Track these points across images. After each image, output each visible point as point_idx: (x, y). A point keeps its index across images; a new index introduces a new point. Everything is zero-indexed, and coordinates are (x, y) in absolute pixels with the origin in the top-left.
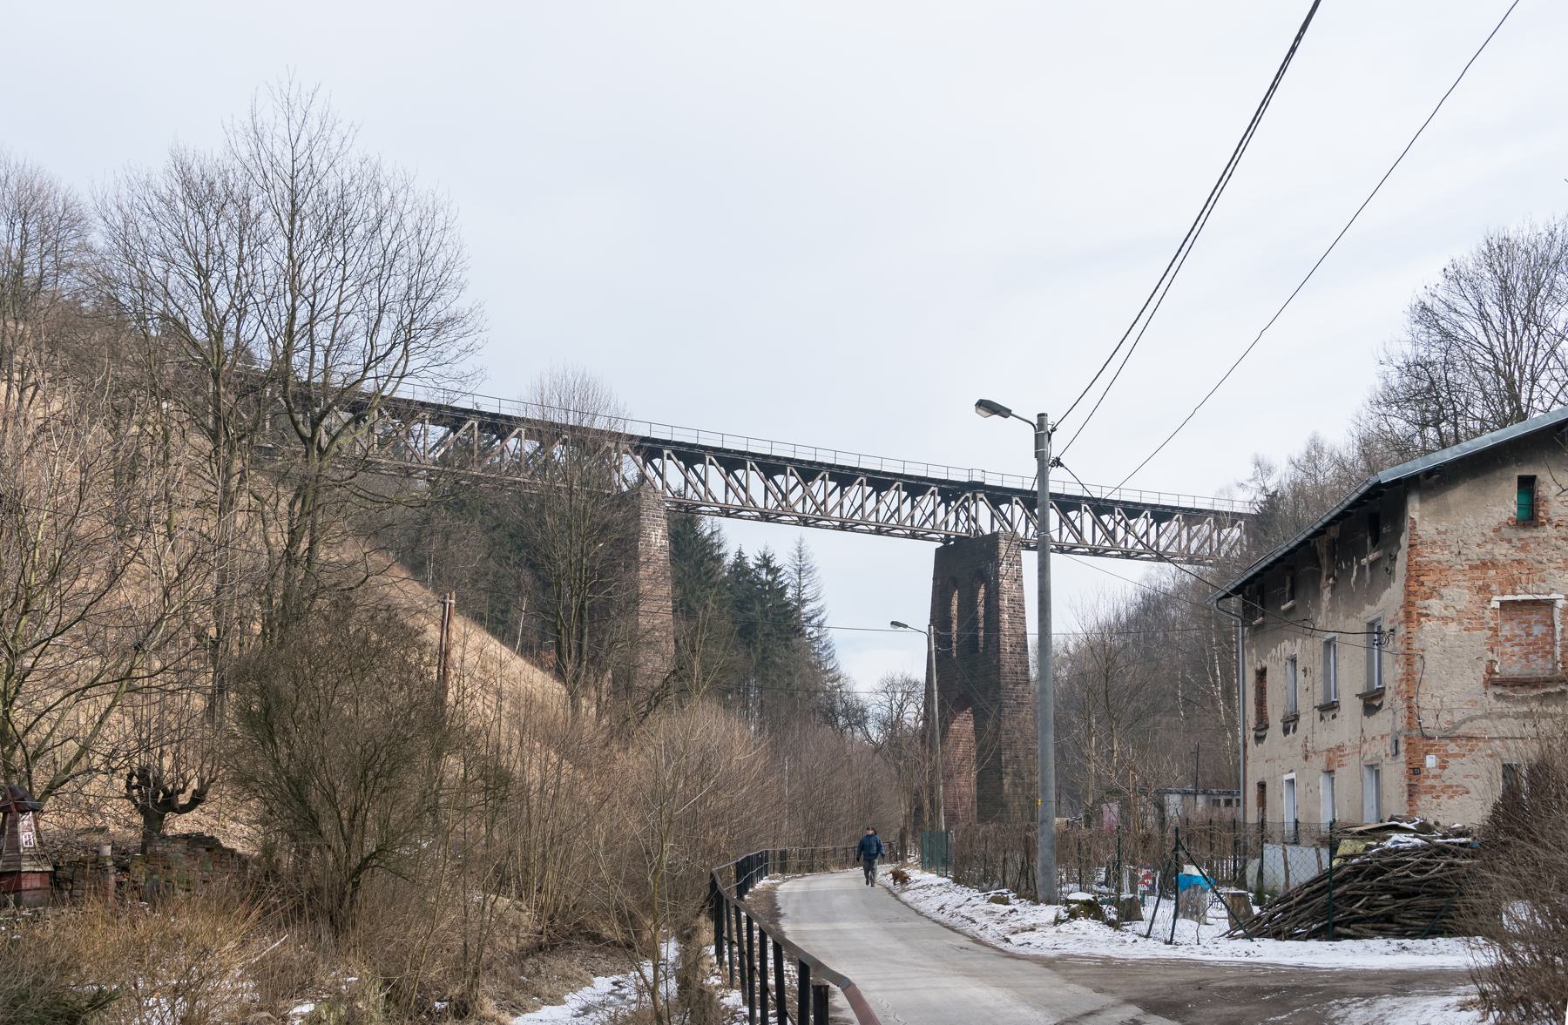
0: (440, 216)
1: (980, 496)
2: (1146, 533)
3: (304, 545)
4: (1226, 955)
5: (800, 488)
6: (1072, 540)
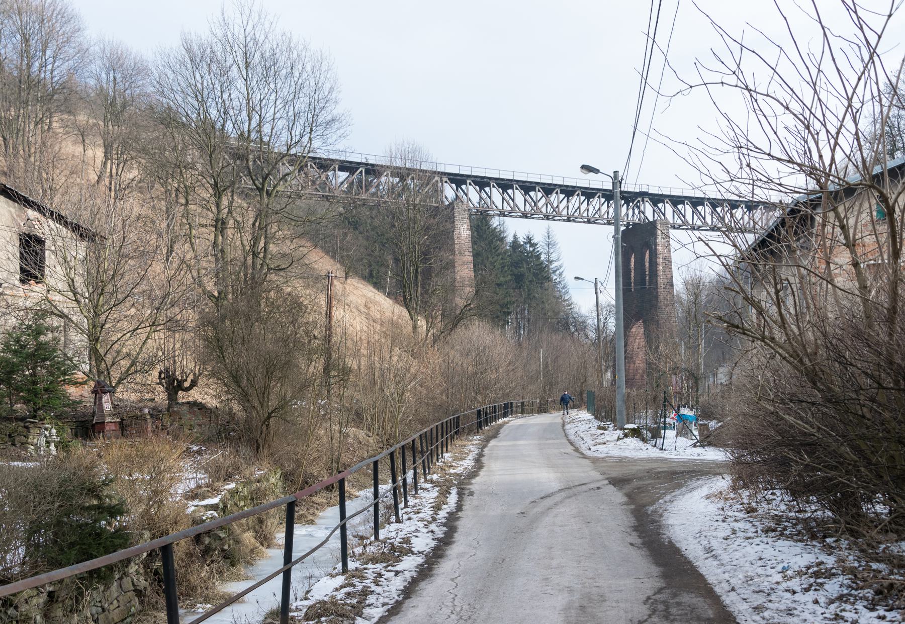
0: (325, 63)
1: (646, 199)
2: (742, 218)
3: (262, 244)
4: (687, 456)
5: (544, 199)
6: (699, 223)
